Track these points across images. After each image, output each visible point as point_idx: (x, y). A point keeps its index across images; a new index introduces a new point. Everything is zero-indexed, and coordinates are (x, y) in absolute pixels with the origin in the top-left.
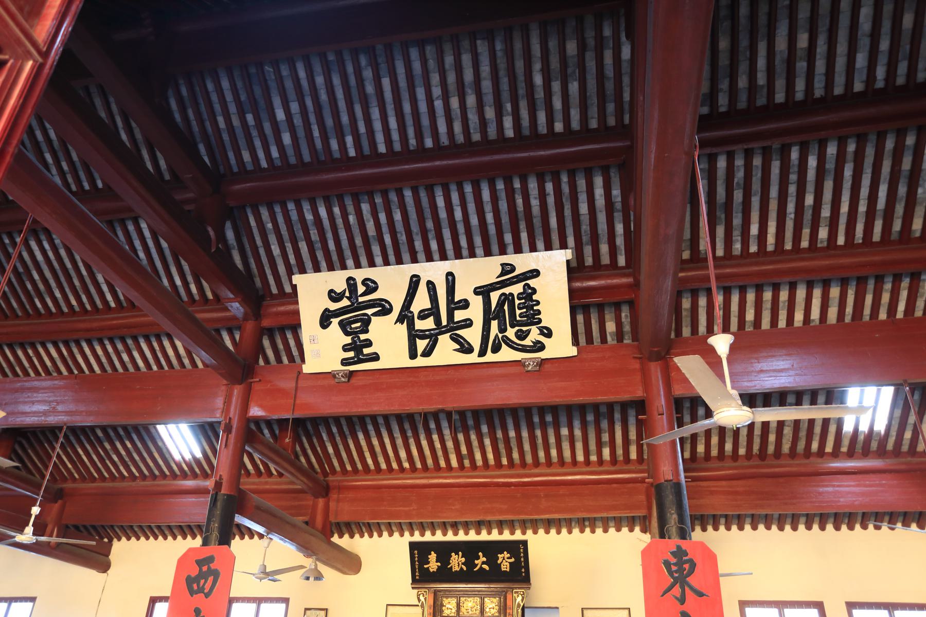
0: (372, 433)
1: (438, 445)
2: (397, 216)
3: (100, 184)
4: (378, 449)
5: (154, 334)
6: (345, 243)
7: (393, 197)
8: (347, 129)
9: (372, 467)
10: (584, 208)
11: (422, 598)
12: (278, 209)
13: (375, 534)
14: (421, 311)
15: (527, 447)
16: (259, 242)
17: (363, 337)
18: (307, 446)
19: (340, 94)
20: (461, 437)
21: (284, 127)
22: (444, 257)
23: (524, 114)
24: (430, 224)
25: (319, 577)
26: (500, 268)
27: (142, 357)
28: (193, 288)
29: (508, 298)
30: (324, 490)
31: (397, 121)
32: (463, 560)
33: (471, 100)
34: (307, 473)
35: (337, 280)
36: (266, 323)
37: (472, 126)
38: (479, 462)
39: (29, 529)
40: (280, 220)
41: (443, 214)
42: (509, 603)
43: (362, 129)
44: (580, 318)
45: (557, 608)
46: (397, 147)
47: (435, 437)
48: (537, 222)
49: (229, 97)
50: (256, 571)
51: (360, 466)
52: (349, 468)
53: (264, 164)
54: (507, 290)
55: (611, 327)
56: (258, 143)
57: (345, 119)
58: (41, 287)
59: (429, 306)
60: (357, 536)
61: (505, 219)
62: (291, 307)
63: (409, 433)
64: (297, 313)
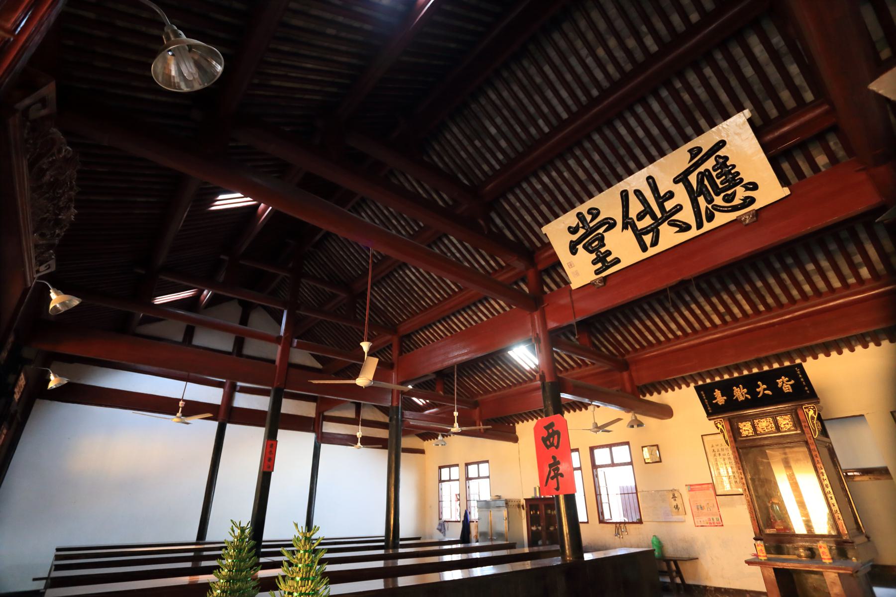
0: (644, 318)
1: (698, 312)
2: (596, 157)
3: (422, 225)
4: (653, 328)
5: (483, 300)
6: (569, 193)
7: (587, 145)
8: (536, 116)
9: (654, 342)
10: (749, 71)
11: (719, 425)
12: (518, 192)
13: (676, 388)
14: (638, 215)
15: (778, 291)
16: (516, 218)
17: (603, 250)
18: (602, 340)
19: (521, 95)
20: (715, 300)
21: (498, 137)
22: (641, 167)
23: (660, 26)
24: (622, 151)
25: (640, 424)
26: (689, 154)
27: (482, 314)
28: (492, 263)
29: (706, 174)
30: (625, 366)
31: (566, 90)
32: (745, 390)
33: (612, 43)
34: (610, 358)
35: (570, 219)
36: (540, 267)
37: (621, 61)
38: (739, 314)
39: (456, 424)
40: (522, 197)
41: (629, 139)
42: (801, 417)
43: (546, 110)
44: (786, 166)
45: (863, 415)
46: (574, 108)
47: (693, 306)
48: (709, 105)
49: (461, 137)
50: (591, 427)
51: (645, 344)
52: (637, 347)
53: (497, 167)
54: (701, 169)
55: (822, 160)
56: (488, 156)
57: (532, 110)
58: (421, 293)
59: (643, 208)
60: (663, 392)
61: (680, 117)
62: (551, 252)
63: (672, 310)
64: (555, 254)
